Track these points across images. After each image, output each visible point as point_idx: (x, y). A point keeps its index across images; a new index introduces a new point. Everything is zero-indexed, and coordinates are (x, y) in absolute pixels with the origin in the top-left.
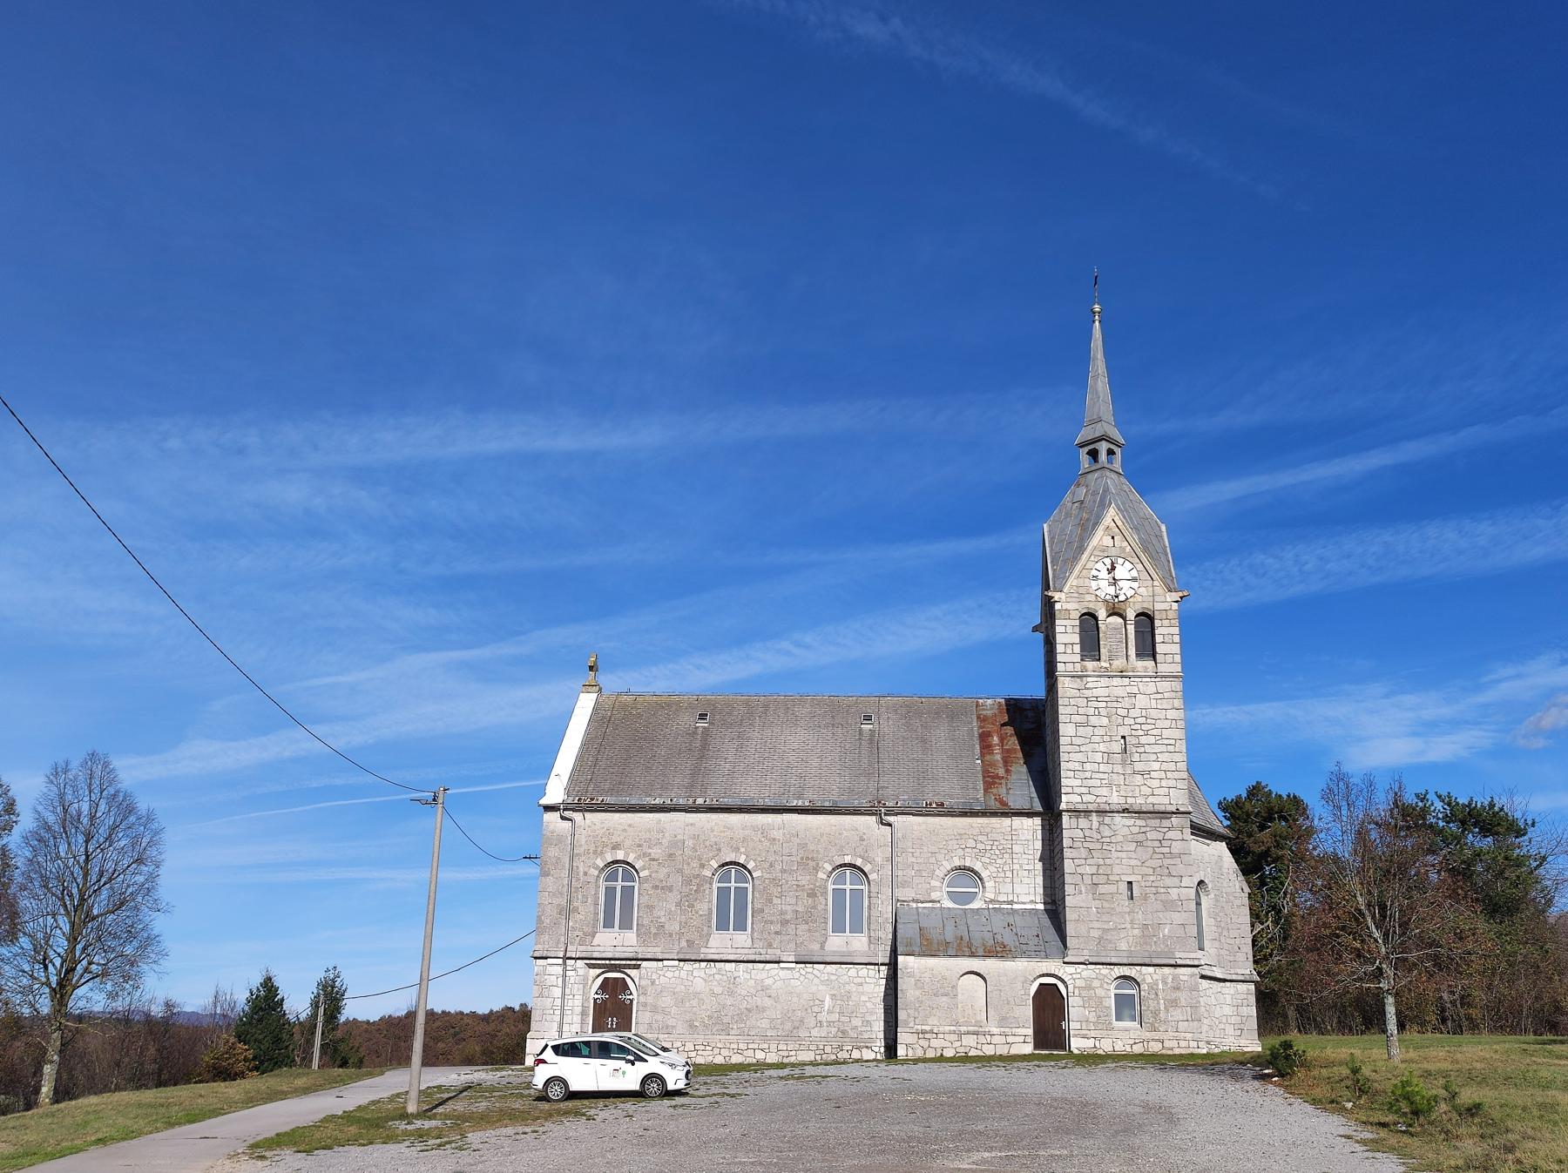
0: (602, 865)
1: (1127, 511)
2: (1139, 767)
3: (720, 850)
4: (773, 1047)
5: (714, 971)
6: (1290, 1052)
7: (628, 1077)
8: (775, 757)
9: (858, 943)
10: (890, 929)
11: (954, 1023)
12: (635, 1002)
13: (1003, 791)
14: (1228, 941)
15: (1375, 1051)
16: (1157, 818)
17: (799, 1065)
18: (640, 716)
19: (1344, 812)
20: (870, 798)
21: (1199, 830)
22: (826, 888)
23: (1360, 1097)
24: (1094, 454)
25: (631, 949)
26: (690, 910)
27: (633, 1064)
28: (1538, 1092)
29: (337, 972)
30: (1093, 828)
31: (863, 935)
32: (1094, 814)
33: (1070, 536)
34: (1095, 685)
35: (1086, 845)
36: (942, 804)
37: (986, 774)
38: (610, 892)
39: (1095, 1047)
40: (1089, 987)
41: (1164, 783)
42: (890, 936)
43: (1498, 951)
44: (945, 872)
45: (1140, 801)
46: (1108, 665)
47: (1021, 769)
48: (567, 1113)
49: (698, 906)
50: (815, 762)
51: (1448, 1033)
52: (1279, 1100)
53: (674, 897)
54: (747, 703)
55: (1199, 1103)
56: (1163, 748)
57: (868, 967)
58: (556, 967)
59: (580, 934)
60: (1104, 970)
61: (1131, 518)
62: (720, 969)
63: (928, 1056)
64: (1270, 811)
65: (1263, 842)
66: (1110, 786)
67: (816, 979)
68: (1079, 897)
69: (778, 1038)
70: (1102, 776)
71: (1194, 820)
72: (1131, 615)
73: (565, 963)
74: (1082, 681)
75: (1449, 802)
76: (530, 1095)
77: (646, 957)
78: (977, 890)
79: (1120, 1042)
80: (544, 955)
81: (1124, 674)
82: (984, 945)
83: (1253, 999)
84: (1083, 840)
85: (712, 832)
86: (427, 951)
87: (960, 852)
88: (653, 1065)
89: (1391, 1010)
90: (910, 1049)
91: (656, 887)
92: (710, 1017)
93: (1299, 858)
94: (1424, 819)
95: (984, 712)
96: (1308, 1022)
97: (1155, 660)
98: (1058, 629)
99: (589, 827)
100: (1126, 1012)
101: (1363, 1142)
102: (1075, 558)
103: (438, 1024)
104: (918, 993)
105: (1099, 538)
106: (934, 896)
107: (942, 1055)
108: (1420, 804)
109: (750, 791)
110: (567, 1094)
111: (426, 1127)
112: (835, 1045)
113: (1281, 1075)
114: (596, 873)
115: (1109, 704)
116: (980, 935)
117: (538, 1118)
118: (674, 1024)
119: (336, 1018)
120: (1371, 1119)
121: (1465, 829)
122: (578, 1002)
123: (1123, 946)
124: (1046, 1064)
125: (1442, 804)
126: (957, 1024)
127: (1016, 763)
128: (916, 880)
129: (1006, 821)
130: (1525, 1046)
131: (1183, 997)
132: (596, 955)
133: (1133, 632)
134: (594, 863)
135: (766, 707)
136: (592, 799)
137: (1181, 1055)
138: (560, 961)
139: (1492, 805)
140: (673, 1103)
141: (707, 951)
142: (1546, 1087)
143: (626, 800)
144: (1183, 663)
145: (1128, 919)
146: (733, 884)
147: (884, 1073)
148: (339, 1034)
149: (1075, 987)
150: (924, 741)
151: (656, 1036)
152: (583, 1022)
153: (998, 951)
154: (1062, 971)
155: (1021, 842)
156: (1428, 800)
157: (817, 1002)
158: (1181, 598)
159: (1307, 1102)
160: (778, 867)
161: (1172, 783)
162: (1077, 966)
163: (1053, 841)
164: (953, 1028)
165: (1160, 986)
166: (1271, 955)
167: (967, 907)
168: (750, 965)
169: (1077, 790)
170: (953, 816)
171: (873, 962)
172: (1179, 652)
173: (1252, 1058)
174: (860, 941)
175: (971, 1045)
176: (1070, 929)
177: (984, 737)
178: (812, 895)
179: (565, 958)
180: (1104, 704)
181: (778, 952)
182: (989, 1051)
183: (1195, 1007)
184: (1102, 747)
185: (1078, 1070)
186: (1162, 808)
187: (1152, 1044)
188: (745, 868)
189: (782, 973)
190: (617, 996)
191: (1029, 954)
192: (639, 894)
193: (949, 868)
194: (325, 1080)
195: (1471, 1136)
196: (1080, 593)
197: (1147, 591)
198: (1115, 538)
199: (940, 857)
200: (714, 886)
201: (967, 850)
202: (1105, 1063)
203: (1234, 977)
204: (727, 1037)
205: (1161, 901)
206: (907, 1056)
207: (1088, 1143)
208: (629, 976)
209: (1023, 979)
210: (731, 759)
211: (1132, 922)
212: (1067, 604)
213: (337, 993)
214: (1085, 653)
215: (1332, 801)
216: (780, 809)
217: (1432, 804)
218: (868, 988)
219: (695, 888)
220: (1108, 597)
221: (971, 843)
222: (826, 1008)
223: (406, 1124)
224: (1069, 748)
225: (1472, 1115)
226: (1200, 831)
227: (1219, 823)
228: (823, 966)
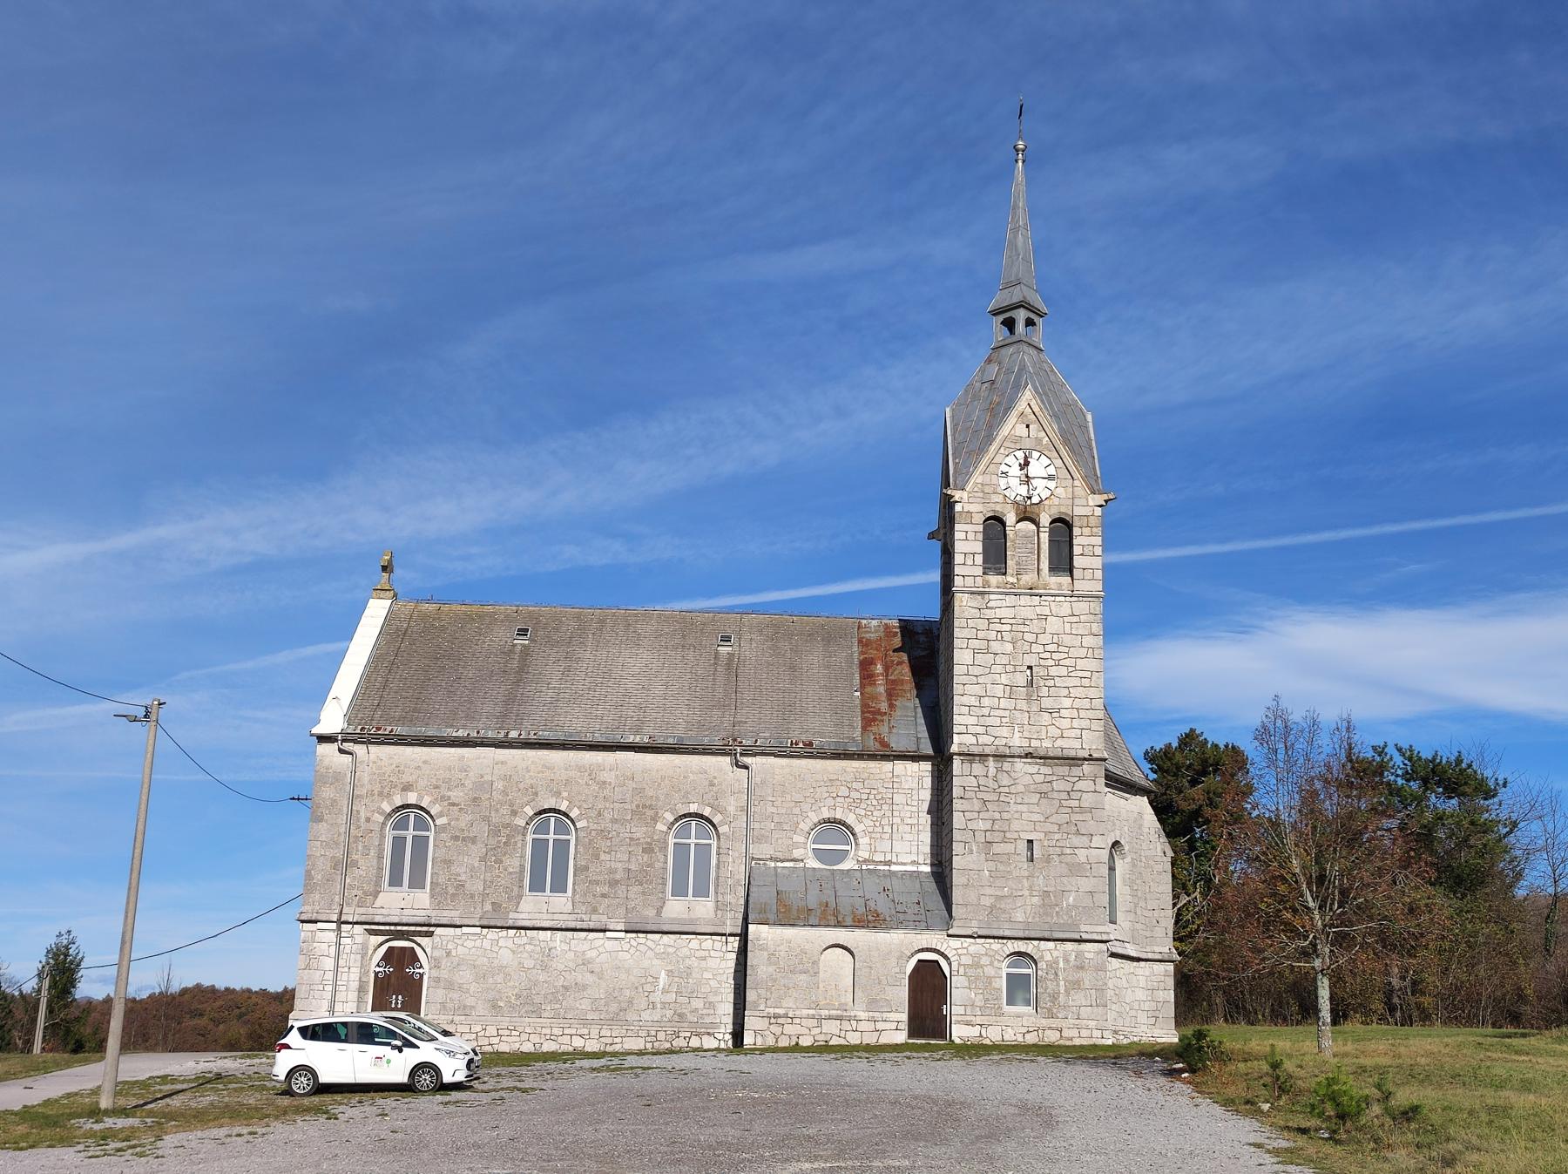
0: (388, 809)
1: (1047, 396)
2: (1046, 703)
3: (536, 794)
4: (594, 1033)
5: (525, 940)
6: (1204, 1043)
7: (394, 1066)
8: (610, 684)
9: (703, 909)
10: (741, 892)
11: (813, 1006)
12: (425, 977)
13: (884, 729)
14: (1146, 913)
15: (1307, 1043)
16: (1065, 765)
17: (622, 1054)
18: (443, 629)
19: (1281, 756)
20: (723, 734)
21: (1117, 781)
22: (666, 842)
23: (1279, 1097)
24: (1010, 324)
25: (423, 913)
26: (497, 866)
27: (401, 1051)
28: (1489, 1092)
29: (71, 937)
30: (990, 775)
31: (709, 899)
32: (991, 759)
33: (977, 424)
34: (999, 603)
35: (980, 795)
36: (811, 744)
37: (865, 707)
38: (399, 843)
39: (981, 1036)
40: (976, 965)
41: (1076, 724)
42: (742, 901)
43: (1457, 931)
44: (811, 825)
45: (1047, 744)
46: (1015, 581)
47: (908, 704)
48: (307, 1110)
49: (507, 861)
50: (658, 689)
51: (1396, 1024)
52: (1185, 1100)
53: (477, 850)
54: (578, 617)
55: (1087, 1103)
56: (1077, 682)
57: (714, 937)
58: (327, 933)
59: (360, 893)
60: (995, 945)
61: (1050, 404)
63: (780, 1044)
64: (1204, 762)
65: (1194, 800)
66: (1012, 725)
68: (969, 858)
69: (601, 1022)
70: (1001, 713)
71: (1111, 769)
72: (1045, 520)
73: (339, 929)
75: (1410, 756)
76: (274, 1088)
77: (441, 922)
78: (848, 848)
79: (1009, 1030)
80: (313, 918)
81: (1033, 591)
82: (853, 913)
83: (1171, 982)
85: (529, 771)
86: (131, 907)
87: (830, 802)
88: (425, 1052)
89: (1324, 993)
90: (759, 1037)
91: (456, 838)
92: (518, 996)
93: (1237, 818)
94: (1381, 774)
95: (867, 636)
96: (1238, 1011)
97: (1072, 576)
98: (958, 535)
99: (374, 762)
100: (1020, 996)
101: (1276, 1152)
102: (982, 450)
103: (219, 1003)
104: (771, 969)
105: (1012, 426)
106: (797, 853)
107: (797, 1044)
108: (1378, 759)
109: (575, 724)
110: (316, 1086)
111: (119, 1126)
113: (1193, 1071)
114: (381, 819)
115: (1014, 628)
116: (849, 901)
117: (268, 1116)
118: (473, 1004)
119: (70, 993)
120: (1290, 1124)
121: (1427, 789)
122: (355, 975)
124: (920, 1055)
125: (1402, 758)
126: (817, 1006)
127: (901, 696)
128: (776, 835)
129: (887, 766)
130: (1480, 1040)
131: (1087, 978)
132: (377, 919)
133: (1047, 541)
134: (379, 808)
135: (602, 622)
136: (379, 729)
137: (1082, 1047)
138: (334, 926)
139: (1459, 761)
140: (447, 1098)
141: (516, 915)
142: (1500, 1086)
143: (420, 731)
144: (1104, 580)
145: (1026, 885)
146: (551, 836)
147: (720, 1065)
148: (74, 1012)
149: (959, 964)
150: (793, 668)
151: (451, 1017)
152: (360, 1000)
153: (870, 920)
154: (945, 945)
155: (903, 791)
156: (1386, 754)
157: (650, 979)
158: (1106, 501)
159: (1217, 1102)
160: (608, 816)
161: (1085, 724)
162: (962, 939)
163: (942, 790)
164: (812, 1012)
165: (1061, 965)
166: (1197, 931)
167: (835, 867)
168: (569, 934)
169: (971, 730)
170: (822, 758)
171: (720, 932)
172: (1101, 567)
173: (1162, 1050)
174: (705, 906)
175: (832, 1032)
176: (957, 895)
177: (866, 666)
178: (648, 850)
179: (340, 922)
180: (1008, 627)
181: (604, 919)
182: (854, 1039)
183: (1101, 990)
184: (1004, 679)
185: (957, 1063)
186: (1072, 754)
187: (1048, 1032)
188: (567, 816)
189: (610, 945)
190: (403, 970)
191: (907, 923)
192: (435, 846)
193: (816, 820)
194: (25, 1067)
195: (1406, 1145)
196: (985, 493)
197: (1066, 493)
198: (1030, 426)
199: (806, 807)
200: (528, 838)
201: (838, 799)
202: (989, 1055)
203: (1150, 956)
204: (538, 1020)
205: (1067, 864)
206: (755, 1044)
207: (937, 1151)
208: (419, 945)
209: (898, 954)
210: (554, 684)
211: (1031, 888)
212: (970, 504)
213: (71, 962)
214: (989, 566)
215: (1267, 743)
216: (613, 746)
217: (1391, 759)
219: (504, 840)
220: (1018, 498)
221: (844, 791)
222: (661, 986)
223: (93, 1123)
224: (965, 679)
225: (1408, 1120)
226: (1117, 782)
227: (1141, 773)
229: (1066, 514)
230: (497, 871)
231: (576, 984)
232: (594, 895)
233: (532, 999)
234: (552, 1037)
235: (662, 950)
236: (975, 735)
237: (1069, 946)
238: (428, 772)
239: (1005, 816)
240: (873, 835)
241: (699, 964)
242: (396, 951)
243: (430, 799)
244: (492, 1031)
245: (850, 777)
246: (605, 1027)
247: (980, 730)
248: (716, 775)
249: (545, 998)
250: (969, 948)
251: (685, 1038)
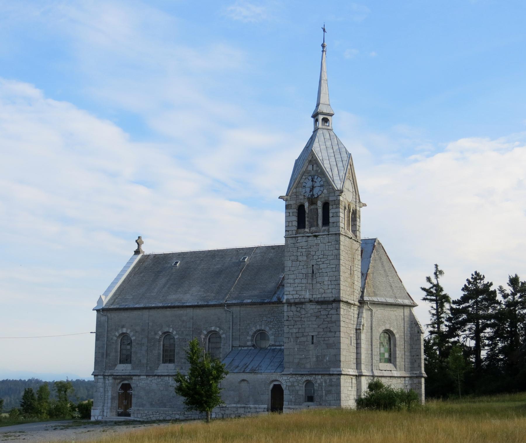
26: (151, 353)
53: (144, 348)
62: (162, 379)
74: (295, 239)
84: (293, 316)
92: (159, 400)
123: (308, 366)
134: (115, 334)
149: (286, 386)
154: (281, 378)
165: (324, 384)
169: (291, 293)
219: (152, 344)
234: (169, 415)
236: (292, 295)
239: (303, 326)
240: (275, 335)
244: (151, 413)
247: (294, 292)
250: (290, 379)
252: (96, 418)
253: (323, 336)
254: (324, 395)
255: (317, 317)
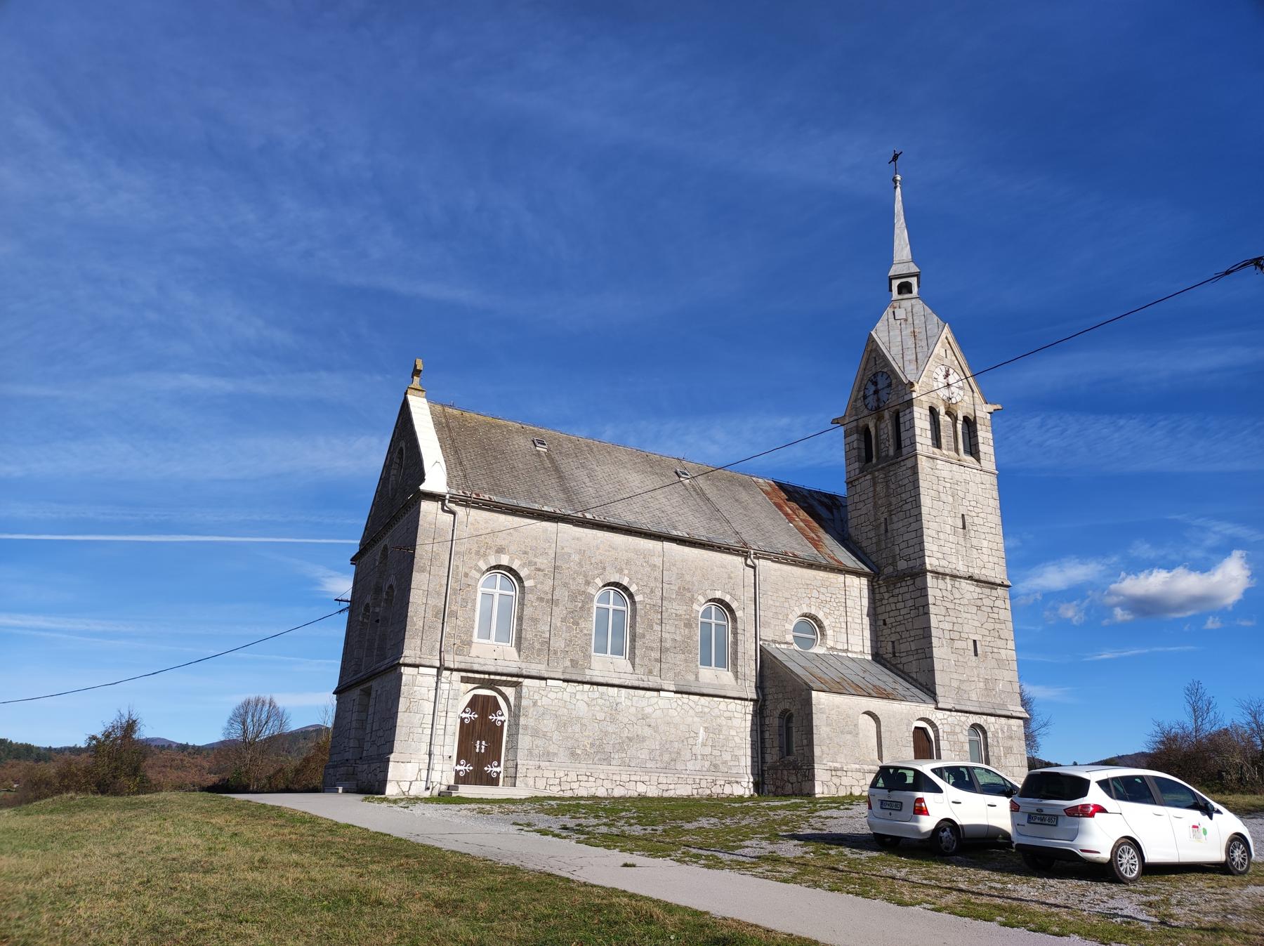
0: (484, 568)
3: (604, 569)
4: (654, 778)
12: (506, 724)
16: (988, 587)
26: (575, 627)
30: (948, 589)
32: (948, 577)
60: (963, 717)
62: (602, 694)
67: (691, 711)
72: (960, 417)
73: (439, 675)
78: (814, 637)
80: (417, 663)
85: (598, 549)
90: (825, 786)
92: (592, 745)
99: (472, 524)
104: (828, 729)
107: (851, 794)
112: (710, 779)
129: (841, 577)
132: (476, 667)
134: (476, 565)
136: (478, 495)
154: (934, 716)
157: (692, 734)
162: (944, 712)
165: (1000, 735)
179: (441, 669)
190: (487, 717)
199: (792, 602)
206: (823, 793)
218: (736, 722)
219: (580, 605)
221: (815, 594)
222: (700, 740)
228: (697, 697)
229: (970, 414)
230: (575, 632)
231: (638, 736)
232: (649, 659)
233: (604, 748)
234: (621, 783)
235: (700, 710)
236: (938, 559)
237: (1003, 720)
238: (518, 539)
241: (727, 722)
242: (480, 699)
243: (520, 563)
244: (573, 776)
245: (818, 584)
246: (662, 775)
247: (940, 555)
248: (732, 570)
249: (614, 747)
251: (720, 786)
252: (405, 787)
253: (991, 644)
254: (1002, 755)
255: (979, 607)
